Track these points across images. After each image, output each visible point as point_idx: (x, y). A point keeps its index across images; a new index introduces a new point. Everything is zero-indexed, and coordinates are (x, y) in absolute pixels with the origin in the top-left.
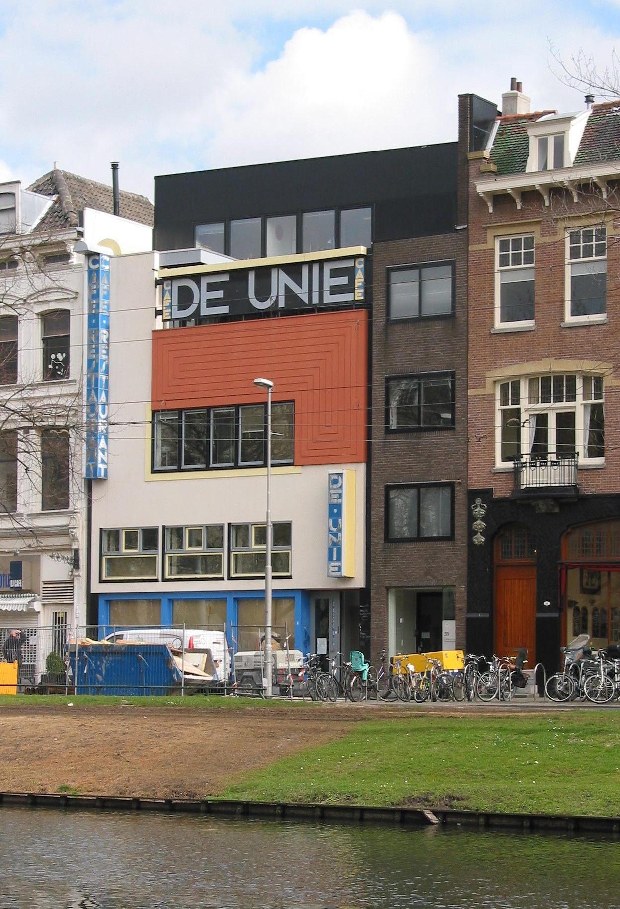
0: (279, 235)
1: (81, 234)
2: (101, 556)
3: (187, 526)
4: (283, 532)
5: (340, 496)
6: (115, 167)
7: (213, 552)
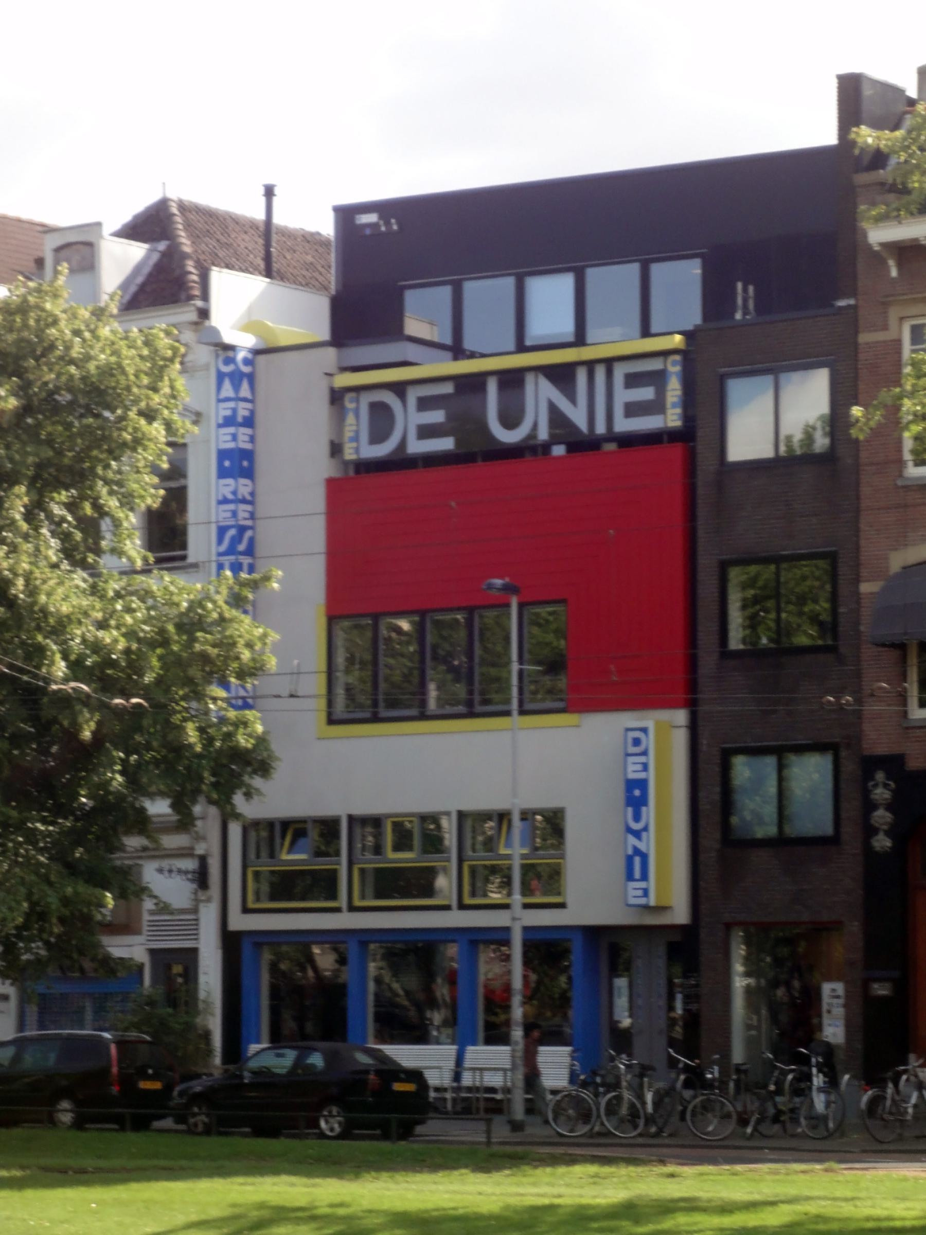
1: (204, 314)
2: (245, 867)
3: (389, 816)
4: (553, 825)
5: (645, 767)
6: (269, 192)
7: (322, 864)
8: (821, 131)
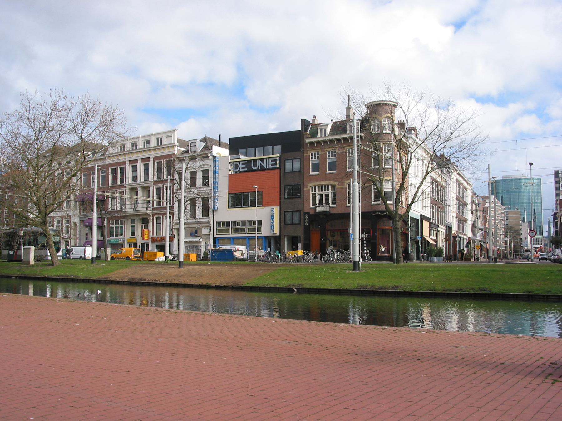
0: (259, 152)
4: (260, 222)
6: (220, 136)
7: (243, 227)
8: (299, 128)
